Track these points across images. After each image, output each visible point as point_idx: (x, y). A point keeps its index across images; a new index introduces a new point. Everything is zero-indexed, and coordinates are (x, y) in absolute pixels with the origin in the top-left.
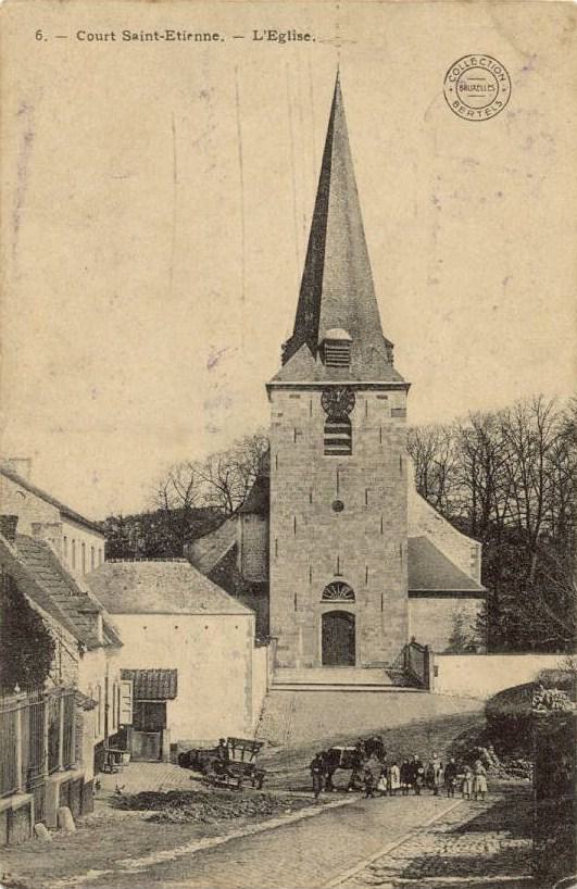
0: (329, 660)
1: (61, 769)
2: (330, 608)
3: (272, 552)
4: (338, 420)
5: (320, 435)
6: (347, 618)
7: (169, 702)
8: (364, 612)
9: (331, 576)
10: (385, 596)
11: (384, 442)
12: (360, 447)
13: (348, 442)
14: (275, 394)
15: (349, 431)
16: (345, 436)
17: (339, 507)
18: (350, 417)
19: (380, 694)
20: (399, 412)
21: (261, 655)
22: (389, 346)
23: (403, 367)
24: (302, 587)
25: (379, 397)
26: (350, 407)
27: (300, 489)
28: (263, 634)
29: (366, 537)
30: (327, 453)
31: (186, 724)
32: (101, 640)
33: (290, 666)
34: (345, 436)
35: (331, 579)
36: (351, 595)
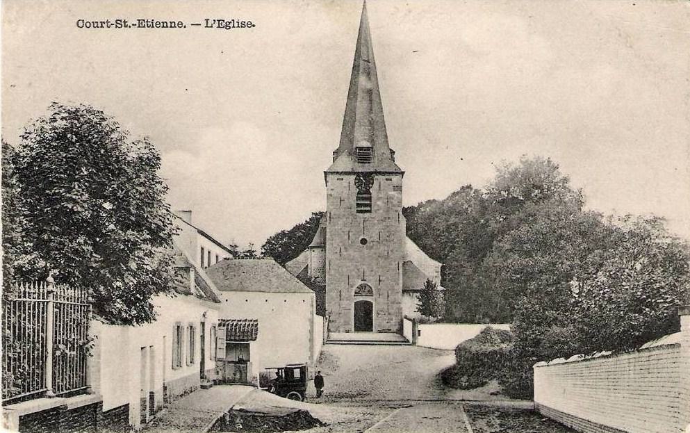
0: (358, 329)
1: (50, 393)
2: (360, 299)
3: (327, 267)
4: (363, 199)
5: (353, 202)
6: (370, 304)
7: (251, 343)
8: (377, 304)
9: (360, 281)
10: (389, 292)
11: (390, 205)
12: (376, 208)
13: (370, 205)
14: (330, 177)
15: (370, 199)
16: (369, 209)
17: (364, 241)
18: (371, 190)
19: (369, 346)
20: (399, 188)
21: (319, 320)
22: (392, 152)
23: (400, 163)
24: (343, 286)
25: (387, 179)
26: (370, 185)
27: (343, 232)
28: (321, 310)
29: (380, 259)
30: (358, 211)
31: (264, 357)
32: (193, 290)
33: (337, 330)
34: (369, 209)
35: (360, 282)
36: (370, 292)
